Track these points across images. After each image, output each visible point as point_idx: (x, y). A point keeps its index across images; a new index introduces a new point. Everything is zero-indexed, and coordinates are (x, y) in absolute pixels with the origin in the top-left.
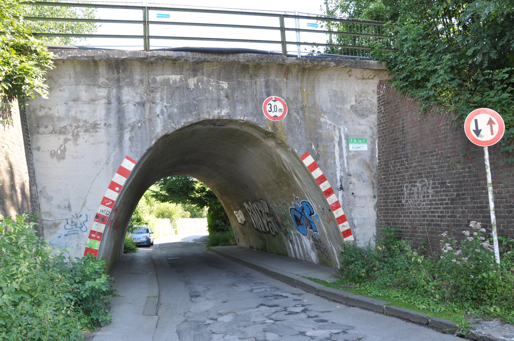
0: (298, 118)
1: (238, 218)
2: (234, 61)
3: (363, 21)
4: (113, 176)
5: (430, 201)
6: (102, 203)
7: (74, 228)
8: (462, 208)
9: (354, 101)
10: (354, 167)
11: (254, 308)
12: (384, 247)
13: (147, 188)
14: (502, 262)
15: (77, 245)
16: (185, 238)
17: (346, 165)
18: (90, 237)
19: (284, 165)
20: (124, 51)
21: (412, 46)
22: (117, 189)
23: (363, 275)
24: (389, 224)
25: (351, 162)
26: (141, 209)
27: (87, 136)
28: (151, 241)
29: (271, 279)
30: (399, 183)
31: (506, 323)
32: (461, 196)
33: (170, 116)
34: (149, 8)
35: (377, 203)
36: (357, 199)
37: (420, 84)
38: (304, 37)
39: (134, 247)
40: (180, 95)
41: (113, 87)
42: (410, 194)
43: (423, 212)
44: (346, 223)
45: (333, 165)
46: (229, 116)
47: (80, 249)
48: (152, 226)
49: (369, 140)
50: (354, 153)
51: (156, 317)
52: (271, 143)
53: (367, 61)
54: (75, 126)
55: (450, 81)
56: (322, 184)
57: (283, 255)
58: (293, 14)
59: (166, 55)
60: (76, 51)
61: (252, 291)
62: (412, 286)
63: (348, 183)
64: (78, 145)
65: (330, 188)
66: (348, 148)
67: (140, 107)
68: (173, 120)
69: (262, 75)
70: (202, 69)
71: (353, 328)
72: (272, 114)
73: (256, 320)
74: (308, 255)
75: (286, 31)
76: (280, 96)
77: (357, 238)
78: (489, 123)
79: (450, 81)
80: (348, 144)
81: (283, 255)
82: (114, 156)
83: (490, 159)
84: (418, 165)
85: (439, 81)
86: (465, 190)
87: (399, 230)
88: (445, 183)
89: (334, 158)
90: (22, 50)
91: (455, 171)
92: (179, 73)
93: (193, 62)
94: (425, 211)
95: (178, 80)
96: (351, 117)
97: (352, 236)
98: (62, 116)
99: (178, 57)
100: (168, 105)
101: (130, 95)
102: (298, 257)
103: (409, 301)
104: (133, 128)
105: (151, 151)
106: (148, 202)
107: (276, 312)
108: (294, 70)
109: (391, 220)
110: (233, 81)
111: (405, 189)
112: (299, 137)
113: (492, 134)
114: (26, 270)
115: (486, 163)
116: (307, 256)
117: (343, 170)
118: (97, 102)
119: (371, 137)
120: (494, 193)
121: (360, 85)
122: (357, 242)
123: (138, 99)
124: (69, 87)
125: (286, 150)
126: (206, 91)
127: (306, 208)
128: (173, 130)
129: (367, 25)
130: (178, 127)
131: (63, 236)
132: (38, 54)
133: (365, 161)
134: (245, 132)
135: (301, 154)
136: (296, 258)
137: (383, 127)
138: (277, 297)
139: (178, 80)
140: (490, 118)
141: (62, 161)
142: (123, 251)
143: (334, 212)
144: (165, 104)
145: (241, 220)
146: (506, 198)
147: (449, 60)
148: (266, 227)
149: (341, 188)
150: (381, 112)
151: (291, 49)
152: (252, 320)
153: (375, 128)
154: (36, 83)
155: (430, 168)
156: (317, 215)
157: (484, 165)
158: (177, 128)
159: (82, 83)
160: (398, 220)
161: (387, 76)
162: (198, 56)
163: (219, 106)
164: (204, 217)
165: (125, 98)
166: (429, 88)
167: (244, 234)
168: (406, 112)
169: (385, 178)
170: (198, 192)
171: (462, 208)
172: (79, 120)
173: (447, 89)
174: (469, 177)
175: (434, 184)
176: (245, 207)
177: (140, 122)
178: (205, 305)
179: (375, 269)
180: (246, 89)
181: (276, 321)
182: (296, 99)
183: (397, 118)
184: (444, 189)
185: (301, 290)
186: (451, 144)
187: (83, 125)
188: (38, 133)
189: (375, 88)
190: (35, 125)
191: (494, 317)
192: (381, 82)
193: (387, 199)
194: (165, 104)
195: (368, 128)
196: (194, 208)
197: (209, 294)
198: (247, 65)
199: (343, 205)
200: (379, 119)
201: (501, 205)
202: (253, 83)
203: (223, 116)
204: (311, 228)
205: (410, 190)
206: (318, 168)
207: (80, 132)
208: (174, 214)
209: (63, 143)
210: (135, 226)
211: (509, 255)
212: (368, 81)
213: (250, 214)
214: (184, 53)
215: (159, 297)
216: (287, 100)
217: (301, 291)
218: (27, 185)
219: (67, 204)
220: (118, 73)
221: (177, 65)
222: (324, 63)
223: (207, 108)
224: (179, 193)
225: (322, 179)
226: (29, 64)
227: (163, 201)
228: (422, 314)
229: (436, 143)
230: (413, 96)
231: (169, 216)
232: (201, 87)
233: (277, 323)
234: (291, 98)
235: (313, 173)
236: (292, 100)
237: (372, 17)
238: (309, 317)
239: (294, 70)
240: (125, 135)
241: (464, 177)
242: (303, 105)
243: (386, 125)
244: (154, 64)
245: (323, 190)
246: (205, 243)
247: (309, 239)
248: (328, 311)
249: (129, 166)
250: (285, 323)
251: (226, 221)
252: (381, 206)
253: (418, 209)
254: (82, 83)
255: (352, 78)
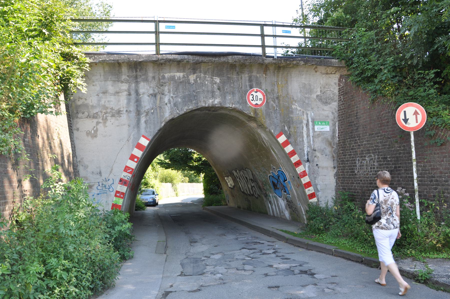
0: (275, 105)
1: (228, 183)
2: (224, 62)
3: (328, 28)
4: (133, 150)
5: (376, 172)
6: (124, 171)
7: (104, 189)
8: (398, 177)
9: (319, 92)
10: (319, 144)
11: (238, 250)
12: (339, 207)
13: (155, 157)
14: (422, 218)
15: (106, 202)
16: (184, 200)
17: (312, 142)
18: (116, 196)
19: (263, 142)
20: (140, 55)
21: (364, 49)
22: (136, 160)
23: (322, 228)
24: (345, 189)
25: (316, 140)
26: (148, 175)
27: (113, 120)
28: (157, 201)
29: (253, 231)
30: (353, 157)
31: (415, 260)
32: (398, 169)
33: (175, 105)
34: (160, 21)
35: (336, 172)
36: (320, 169)
37: (370, 79)
38: (280, 41)
39: (143, 206)
40: (183, 88)
41: (132, 82)
42: (361, 166)
43: (370, 180)
44: (311, 188)
45: (301, 143)
46: (221, 104)
47: (108, 204)
48: (157, 189)
49: (331, 123)
50: (319, 133)
51: (165, 255)
52: (253, 125)
53: (330, 60)
54: (104, 112)
55: (392, 78)
56: (293, 157)
57: (263, 213)
58: (271, 23)
59: (172, 58)
60: (105, 56)
61: (237, 239)
62: (356, 236)
63: (313, 157)
64: (106, 127)
65: (299, 160)
66: (313, 129)
67: (152, 98)
68: (177, 107)
69: (246, 72)
70: (200, 68)
71: (308, 263)
72: (254, 103)
73: (238, 257)
74: (283, 213)
75: (265, 37)
76: (260, 88)
77: (320, 200)
78: (414, 114)
79: (392, 78)
80: (314, 126)
81: (263, 213)
82: (134, 135)
83: (415, 141)
84: (368, 143)
85: (384, 78)
86: (400, 164)
87: (352, 194)
88: (386, 158)
89: (303, 137)
90: (67, 57)
91: (393, 149)
92: (182, 71)
93: (193, 63)
94: (372, 179)
95: (181, 77)
96: (317, 105)
97: (316, 198)
98: (95, 105)
99: (182, 59)
100: (174, 96)
101: (145, 89)
102: (276, 215)
103: (353, 246)
104: (147, 114)
105: (161, 131)
106: (154, 169)
107: (254, 253)
108: (272, 68)
109: (346, 186)
110: (224, 77)
111: (357, 162)
112: (275, 120)
113: (417, 122)
114: (84, 216)
115: (412, 144)
116: (282, 214)
117: (309, 146)
118: (120, 94)
119: (333, 120)
120: (417, 166)
121: (324, 79)
122: (320, 203)
123: (151, 92)
124: (100, 82)
125: (265, 131)
126: (203, 84)
127: (281, 175)
128: (178, 115)
129: (329, 30)
130: (182, 113)
131: (96, 195)
132: (78, 59)
133: (328, 139)
134: (233, 116)
135: (276, 134)
136: (274, 216)
137: (342, 112)
138: (256, 243)
139: (181, 77)
140: (416, 110)
141: (95, 139)
142: (134, 209)
143: (302, 179)
144: (172, 95)
145: (231, 185)
146: (429, 170)
147: (392, 62)
148: (251, 190)
149: (308, 161)
150: (341, 100)
151: (269, 52)
152: (235, 257)
153: (336, 113)
154: (78, 82)
155: (376, 146)
156: (289, 182)
157: (411, 145)
158: (181, 114)
159: (109, 80)
160: (352, 186)
161: (346, 71)
162: (197, 58)
163: (213, 97)
164: (200, 182)
165: (141, 91)
166: (376, 83)
167: (233, 196)
168: (360, 101)
169: (343, 153)
170: (195, 162)
171: (398, 177)
172: (107, 108)
173: (389, 85)
174: (404, 153)
175: (379, 158)
176: (234, 174)
177: (152, 109)
178: (201, 248)
179: (331, 223)
180: (233, 83)
181: (253, 258)
182: (273, 90)
183: (353, 106)
184: (386, 162)
185: (274, 239)
186: (391, 128)
187: (110, 112)
188: (77, 117)
189: (337, 81)
190: (75, 112)
191: (409, 257)
192: (341, 76)
193: (344, 169)
194: (172, 95)
195: (331, 113)
196: (192, 174)
197: (204, 241)
198: (235, 65)
199: (309, 173)
200: (339, 106)
201: (426, 175)
202: (240, 79)
203: (216, 104)
204: (285, 192)
205: (361, 163)
206: (290, 145)
207: (108, 116)
208: (174, 179)
209: (95, 125)
210: (143, 189)
211: (428, 213)
212: (331, 75)
213: (238, 180)
214: (186, 56)
215: (166, 242)
216: (266, 91)
217: (274, 239)
218: (71, 155)
219: (99, 171)
220: (136, 71)
221: (181, 65)
222: (295, 62)
223: (204, 98)
224: (180, 162)
225: (293, 153)
226: (73, 68)
227: (166, 168)
228: (359, 255)
229: (381, 127)
230: (364, 89)
231: (171, 181)
232: (199, 81)
233: (253, 259)
234: (269, 90)
235: (285, 149)
236: (270, 91)
237: (335, 24)
238: (277, 256)
239: (272, 68)
240: (142, 119)
241: (400, 153)
242: (279, 95)
243: (345, 111)
244: (163, 65)
245: (293, 162)
246: (202, 204)
247: (284, 200)
248: (292, 253)
249: (145, 142)
250: (259, 260)
251: (219, 185)
252: (339, 175)
253: (366, 178)
254: (109, 80)
255: (318, 73)
